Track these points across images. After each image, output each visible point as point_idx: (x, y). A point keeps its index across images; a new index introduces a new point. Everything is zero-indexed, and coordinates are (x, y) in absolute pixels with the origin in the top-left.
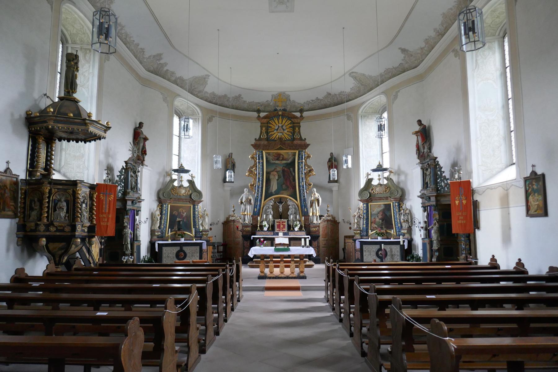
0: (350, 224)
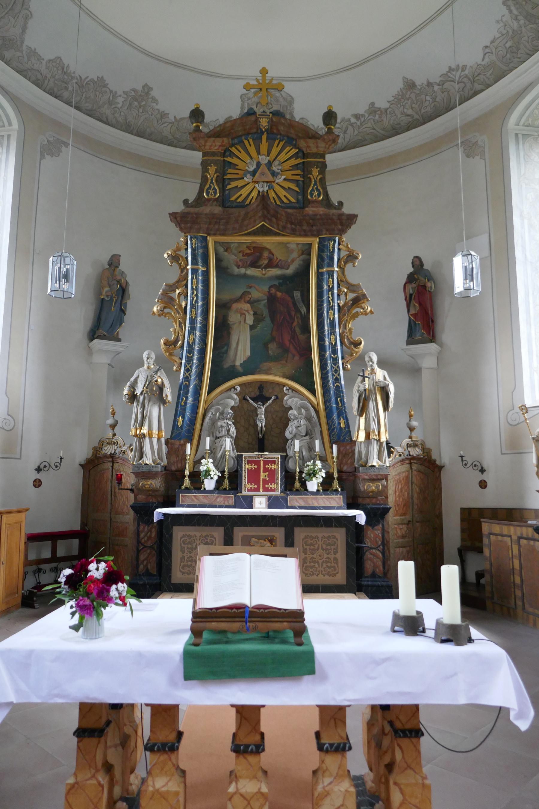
0: (482, 471)
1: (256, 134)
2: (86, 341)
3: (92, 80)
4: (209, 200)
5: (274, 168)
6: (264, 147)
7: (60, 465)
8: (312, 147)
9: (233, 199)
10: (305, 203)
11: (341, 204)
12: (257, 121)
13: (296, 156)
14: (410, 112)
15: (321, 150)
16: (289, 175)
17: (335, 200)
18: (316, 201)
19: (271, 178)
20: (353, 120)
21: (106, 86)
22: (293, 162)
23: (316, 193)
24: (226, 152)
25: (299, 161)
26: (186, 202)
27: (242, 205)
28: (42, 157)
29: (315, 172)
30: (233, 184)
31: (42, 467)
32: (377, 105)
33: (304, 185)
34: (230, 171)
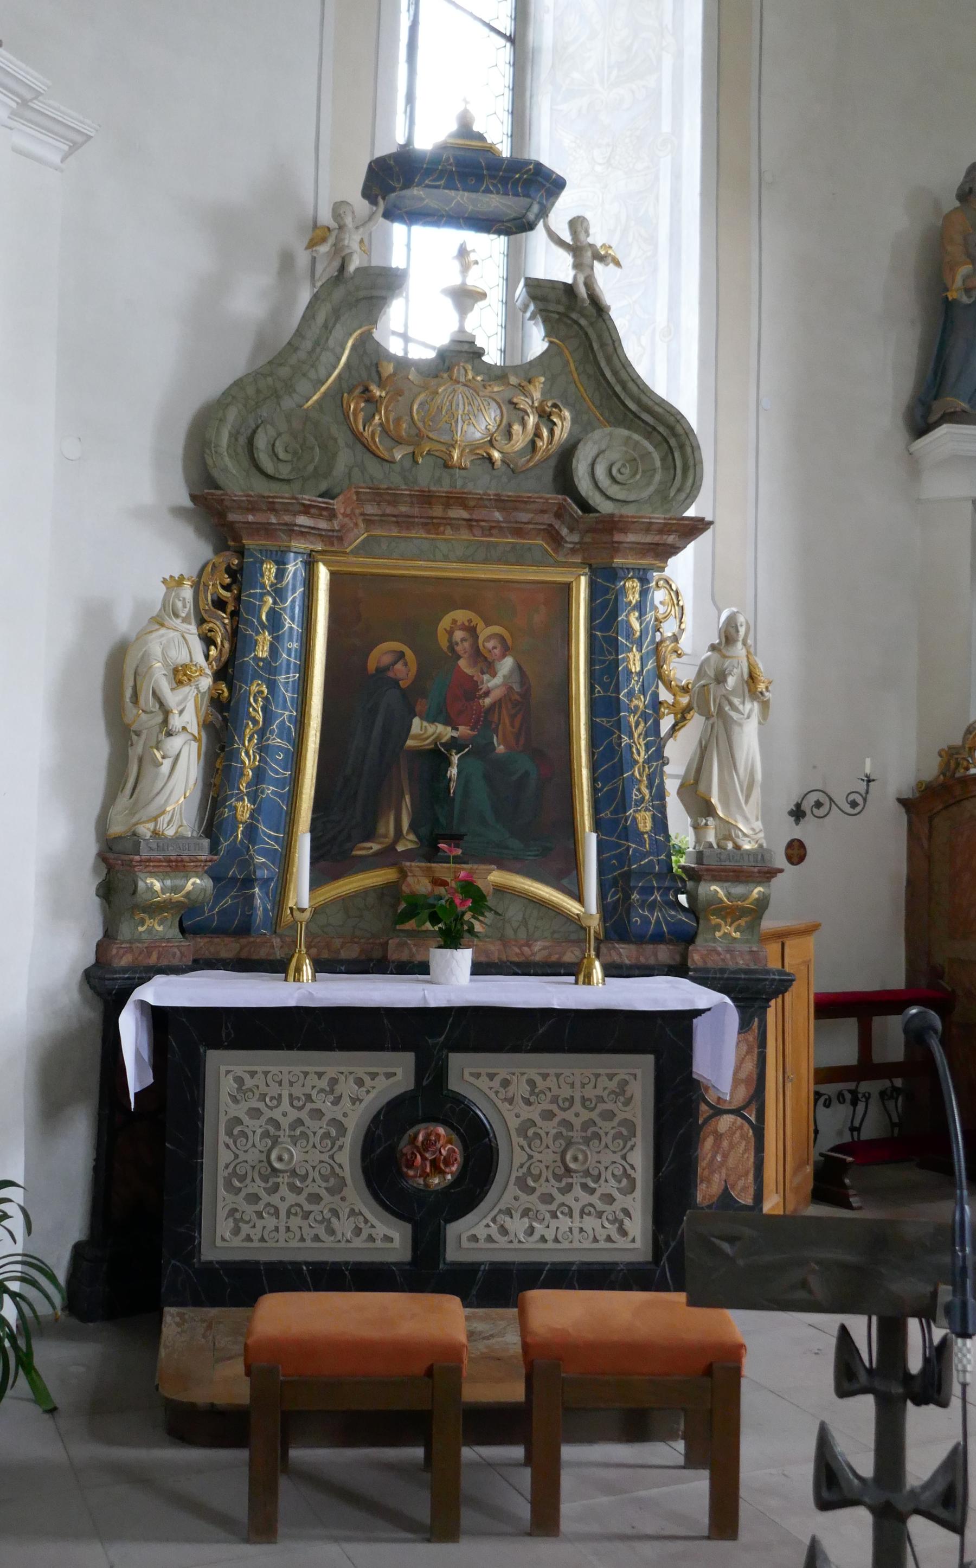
2: (900, 434)
7: (865, 800)
31: (806, 806)
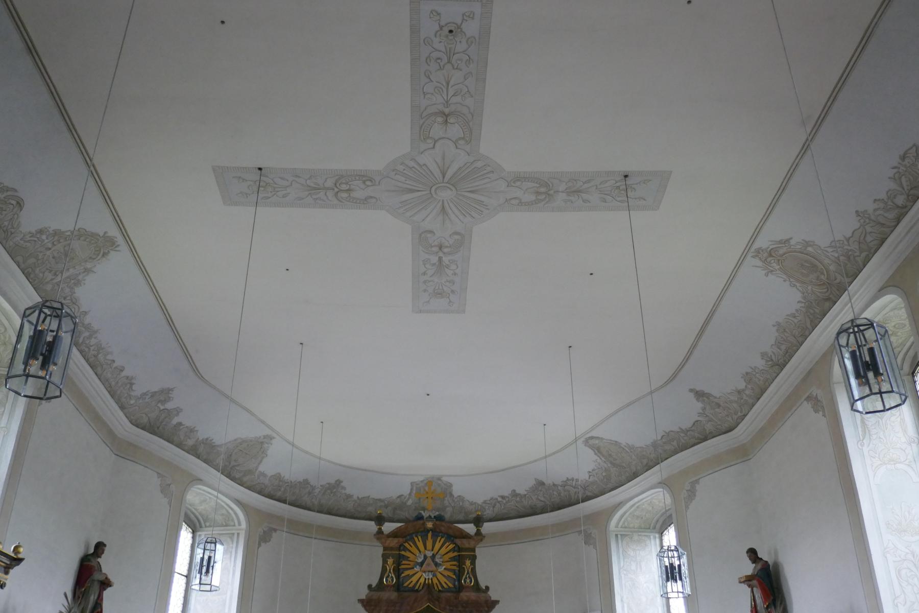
1: (424, 533)
3: (300, 482)
4: (388, 586)
5: (438, 560)
6: (429, 543)
8: (465, 543)
9: (405, 585)
10: (460, 588)
11: (487, 588)
12: (424, 524)
13: (453, 550)
14: (542, 499)
15: (472, 546)
16: (448, 565)
17: (483, 585)
18: (468, 587)
19: (434, 568)
20: (500, 499)
21: (308, 483)
22: (452, 555)
23: (468, 581)
24: (401, 547)
25: (456, 554)
26: (370, 587)
27: (413, 590)
28: (259, 545)
29: (468, 563)
30: (406, 573)
32: (517, 492)
33: (460, 574)
34: (404, 562)
